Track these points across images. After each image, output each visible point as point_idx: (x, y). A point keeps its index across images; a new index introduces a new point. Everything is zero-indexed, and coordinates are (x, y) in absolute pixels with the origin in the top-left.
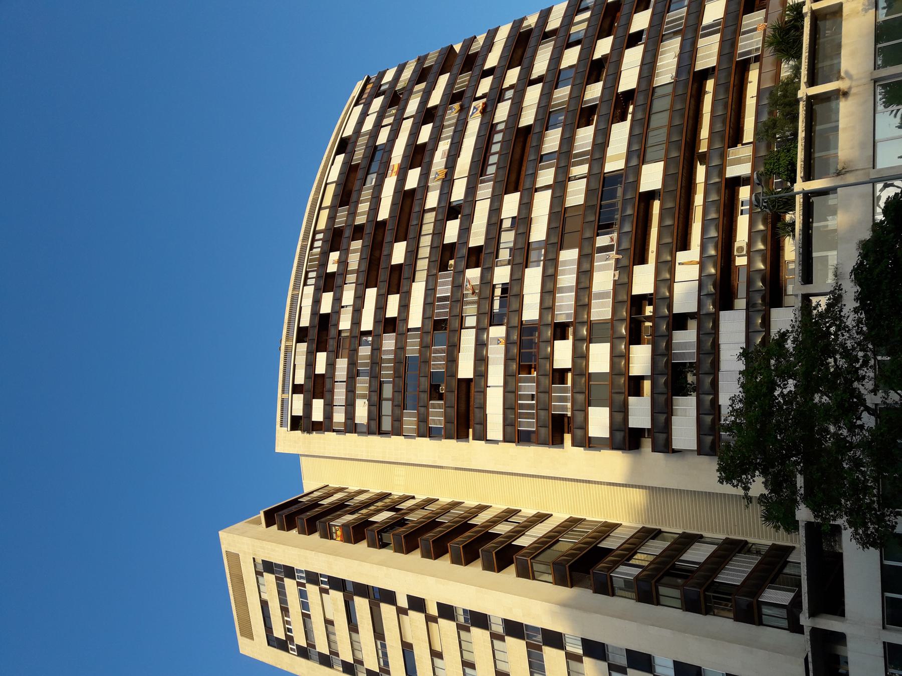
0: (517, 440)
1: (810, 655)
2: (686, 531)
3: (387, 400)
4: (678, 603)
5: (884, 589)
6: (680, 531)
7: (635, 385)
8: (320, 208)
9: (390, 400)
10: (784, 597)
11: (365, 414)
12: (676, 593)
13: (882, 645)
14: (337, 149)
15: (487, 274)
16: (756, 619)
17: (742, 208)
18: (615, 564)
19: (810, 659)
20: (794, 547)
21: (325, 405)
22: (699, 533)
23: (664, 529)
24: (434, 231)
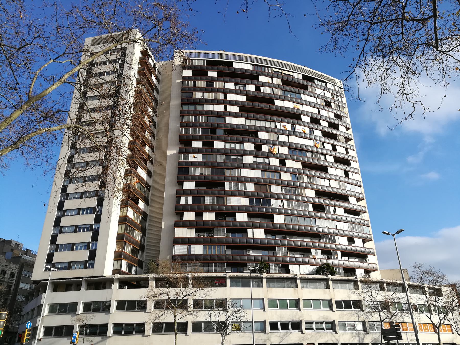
0: (177, 196)
1: (105, 278)
2: (147, 231)
3: (189, 107)
4: (120, 232)
5: (128, 301)
6: (147, 228)
7: (199, 215)
8: (293, 72)
9: (188, 109)
10: (124, 268)
11: (232, 203)
12: (123, 231)
13: (110, 300)
14: (310, 76)
15: (249, 153)
16: (116, 259)
17: (315, 329)
18: (133, 208)
19: (104, 278)
20: (143, 269)
21: (236, 113)
22: (146, 235)
23: (147, 222)
24: (267, 127)
